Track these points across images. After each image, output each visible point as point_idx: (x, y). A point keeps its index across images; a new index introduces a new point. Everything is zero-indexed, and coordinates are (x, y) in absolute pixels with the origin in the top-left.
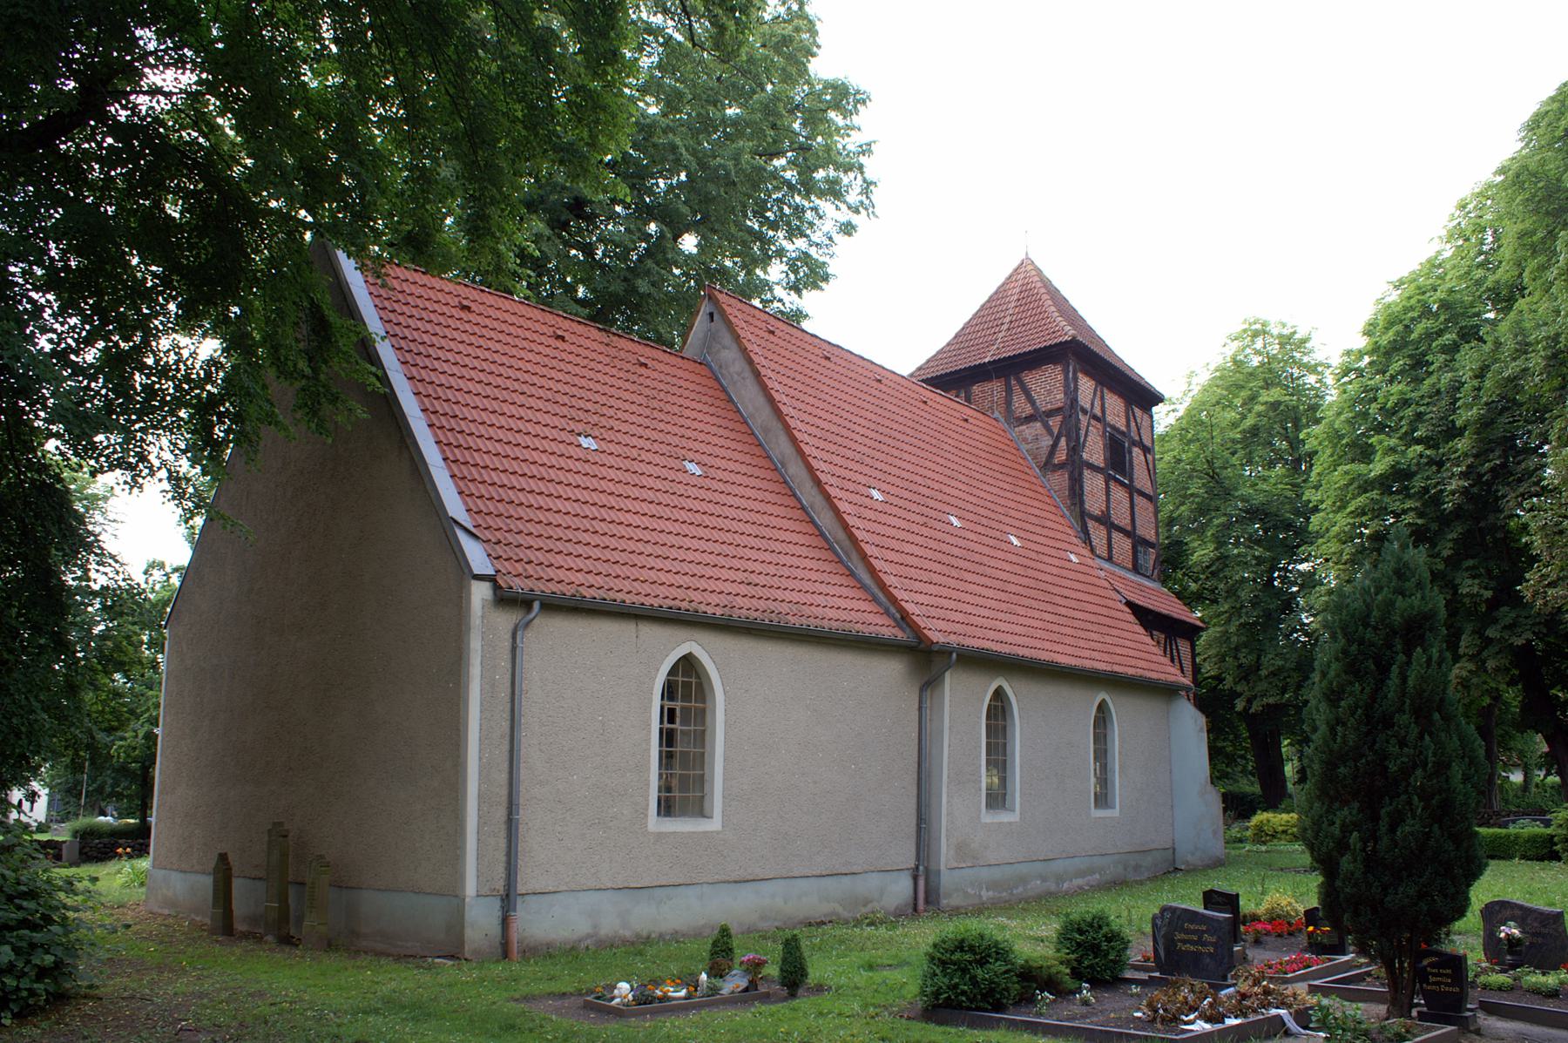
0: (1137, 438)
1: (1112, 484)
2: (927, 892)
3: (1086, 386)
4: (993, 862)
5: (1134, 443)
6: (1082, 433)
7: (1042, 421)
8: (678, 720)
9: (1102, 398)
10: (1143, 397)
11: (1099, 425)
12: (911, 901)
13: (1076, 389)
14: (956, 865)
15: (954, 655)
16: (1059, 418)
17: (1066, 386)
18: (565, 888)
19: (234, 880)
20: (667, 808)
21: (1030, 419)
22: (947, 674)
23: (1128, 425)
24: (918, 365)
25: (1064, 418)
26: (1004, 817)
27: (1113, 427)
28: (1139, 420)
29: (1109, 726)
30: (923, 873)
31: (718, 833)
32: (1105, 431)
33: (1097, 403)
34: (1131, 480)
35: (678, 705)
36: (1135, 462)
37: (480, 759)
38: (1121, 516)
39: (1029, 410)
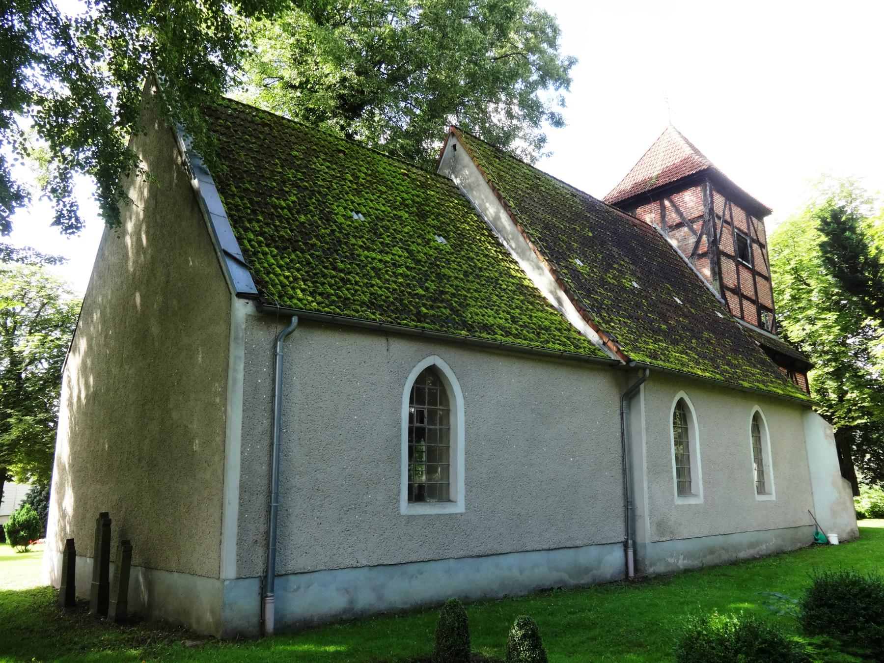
0: (755, 238)
1: (741, 268)
2: (636, 561)
3: (719, 201)
4: (687, 536)
5: (753, 241)
6: (718, 231)
7: (688, 226)
8: (426, 420)
9: (730, 209)
10: (757, 211)
11: (729, 227)
12: (623, 568)
13: (712, 202)
14: (657, 539)
15: (648, 372)
16: (701, 222)
17: (705, 200)
18: (323, 567)
19: (77, 559)
20: (417, 494)
21: (679, 225)
22: (642, 387)
23: (749, 228)
24: (572, 323)
25: (704, 222)
26: (692, 501)
27: (739, 229)
28: (756, 226)
29: (761, 429)
30: (630, 542)
31: (461, 514)
32: (733, 232)
33: (727, 212)
34: (753, 265)
35: (426, 408)
36: (755, 254)
37: (242, 453)
38: (748, 290)
39: (677, 220)
